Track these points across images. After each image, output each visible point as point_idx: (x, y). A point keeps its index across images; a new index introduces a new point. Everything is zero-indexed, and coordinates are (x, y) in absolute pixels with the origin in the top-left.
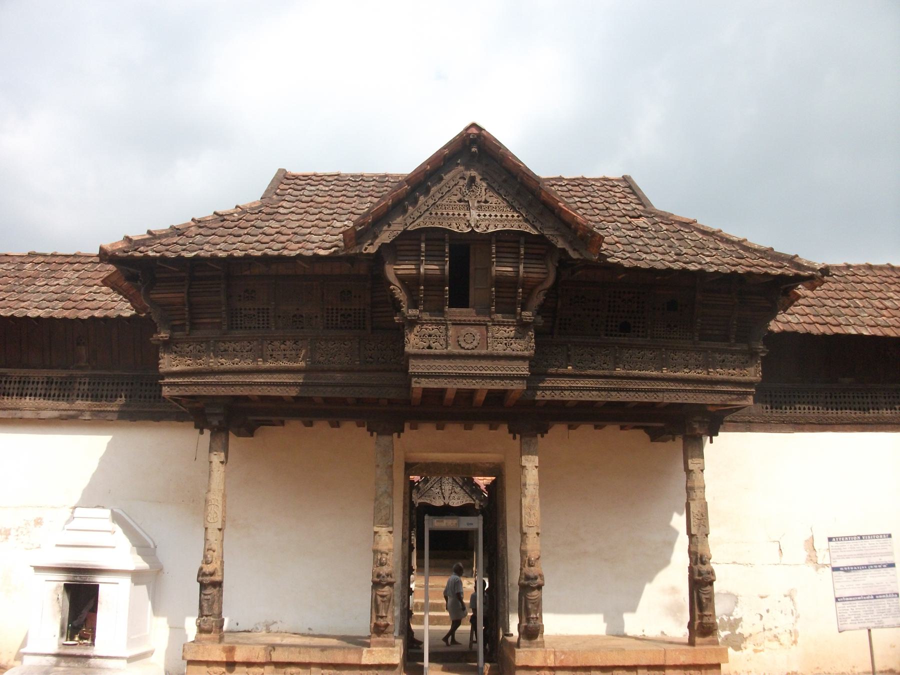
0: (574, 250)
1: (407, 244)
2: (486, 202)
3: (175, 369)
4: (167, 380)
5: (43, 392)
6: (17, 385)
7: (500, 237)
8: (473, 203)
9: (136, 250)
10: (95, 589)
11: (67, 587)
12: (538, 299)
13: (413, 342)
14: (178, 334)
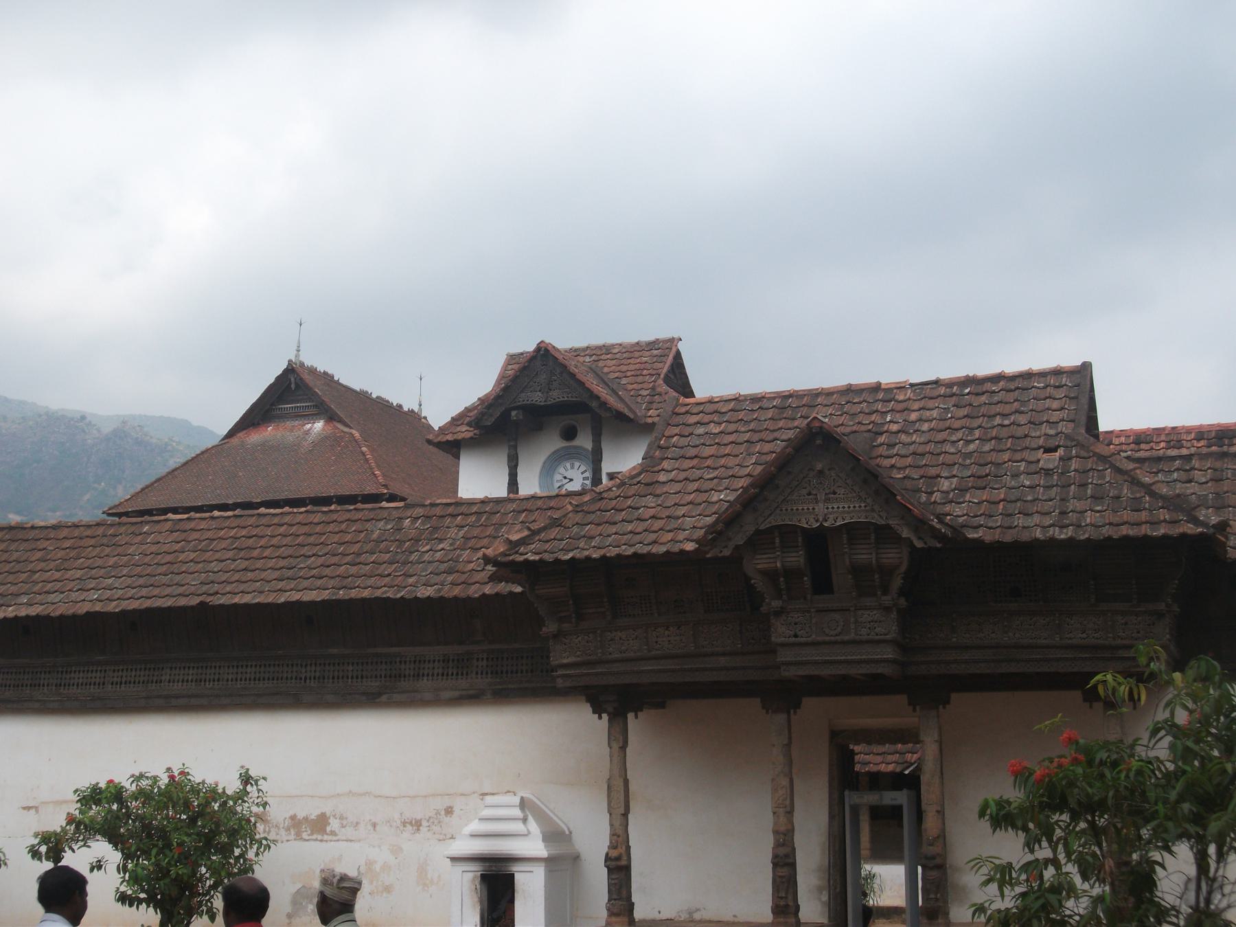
0: (920, 538)
1: (759, 541)
2: (835, 493)
3: (565, 661)
4: (559, 672)
5: (440, 671)
6: (412, 666)
7: (850, 528)
8: (821, 496)
9: (517, 552)
10: (511, 877)
11: (484, 878)
12: (897, 582)
13: (781, 632)
14: (566, 626)
